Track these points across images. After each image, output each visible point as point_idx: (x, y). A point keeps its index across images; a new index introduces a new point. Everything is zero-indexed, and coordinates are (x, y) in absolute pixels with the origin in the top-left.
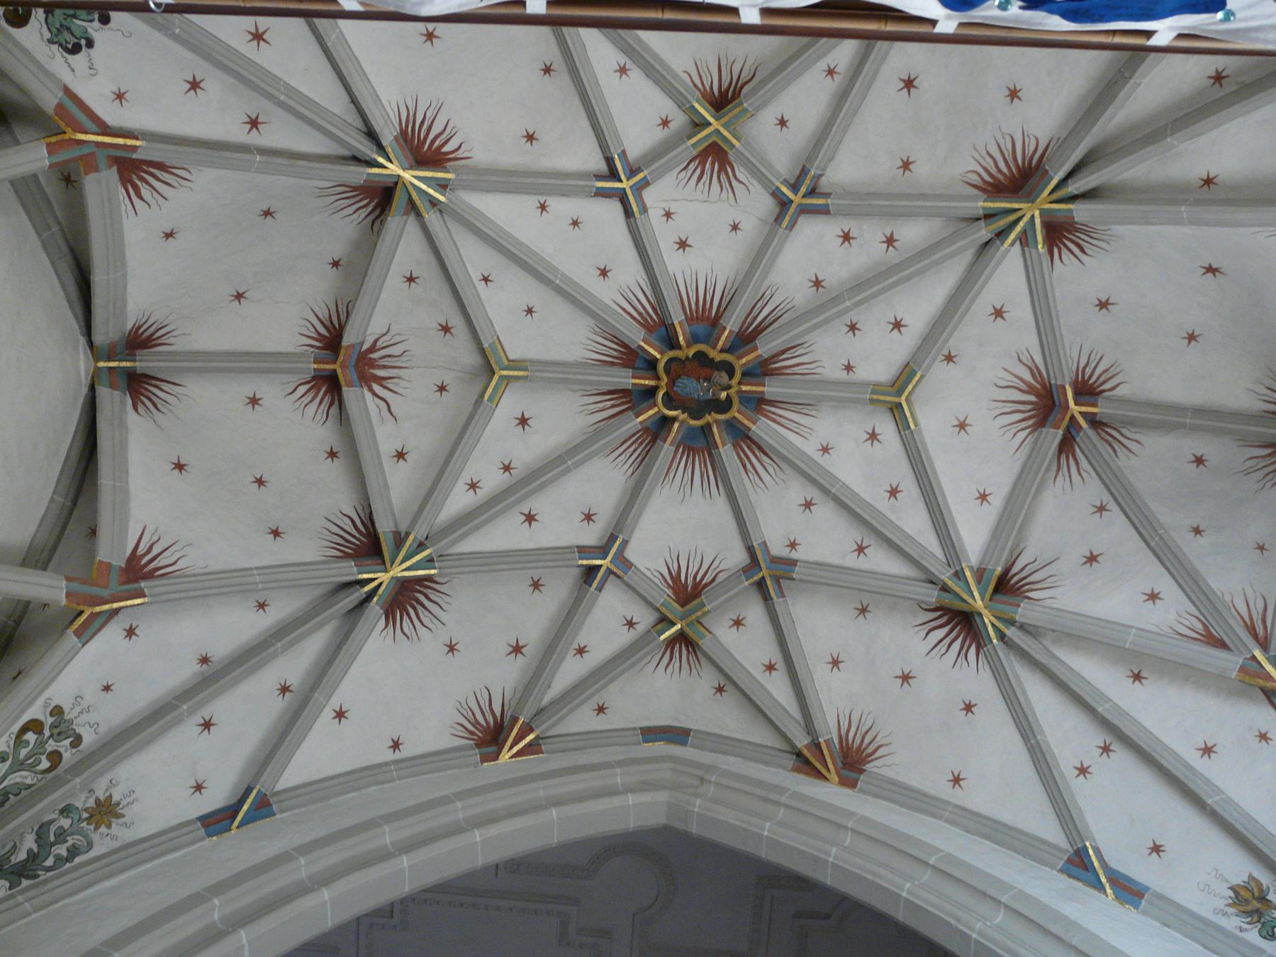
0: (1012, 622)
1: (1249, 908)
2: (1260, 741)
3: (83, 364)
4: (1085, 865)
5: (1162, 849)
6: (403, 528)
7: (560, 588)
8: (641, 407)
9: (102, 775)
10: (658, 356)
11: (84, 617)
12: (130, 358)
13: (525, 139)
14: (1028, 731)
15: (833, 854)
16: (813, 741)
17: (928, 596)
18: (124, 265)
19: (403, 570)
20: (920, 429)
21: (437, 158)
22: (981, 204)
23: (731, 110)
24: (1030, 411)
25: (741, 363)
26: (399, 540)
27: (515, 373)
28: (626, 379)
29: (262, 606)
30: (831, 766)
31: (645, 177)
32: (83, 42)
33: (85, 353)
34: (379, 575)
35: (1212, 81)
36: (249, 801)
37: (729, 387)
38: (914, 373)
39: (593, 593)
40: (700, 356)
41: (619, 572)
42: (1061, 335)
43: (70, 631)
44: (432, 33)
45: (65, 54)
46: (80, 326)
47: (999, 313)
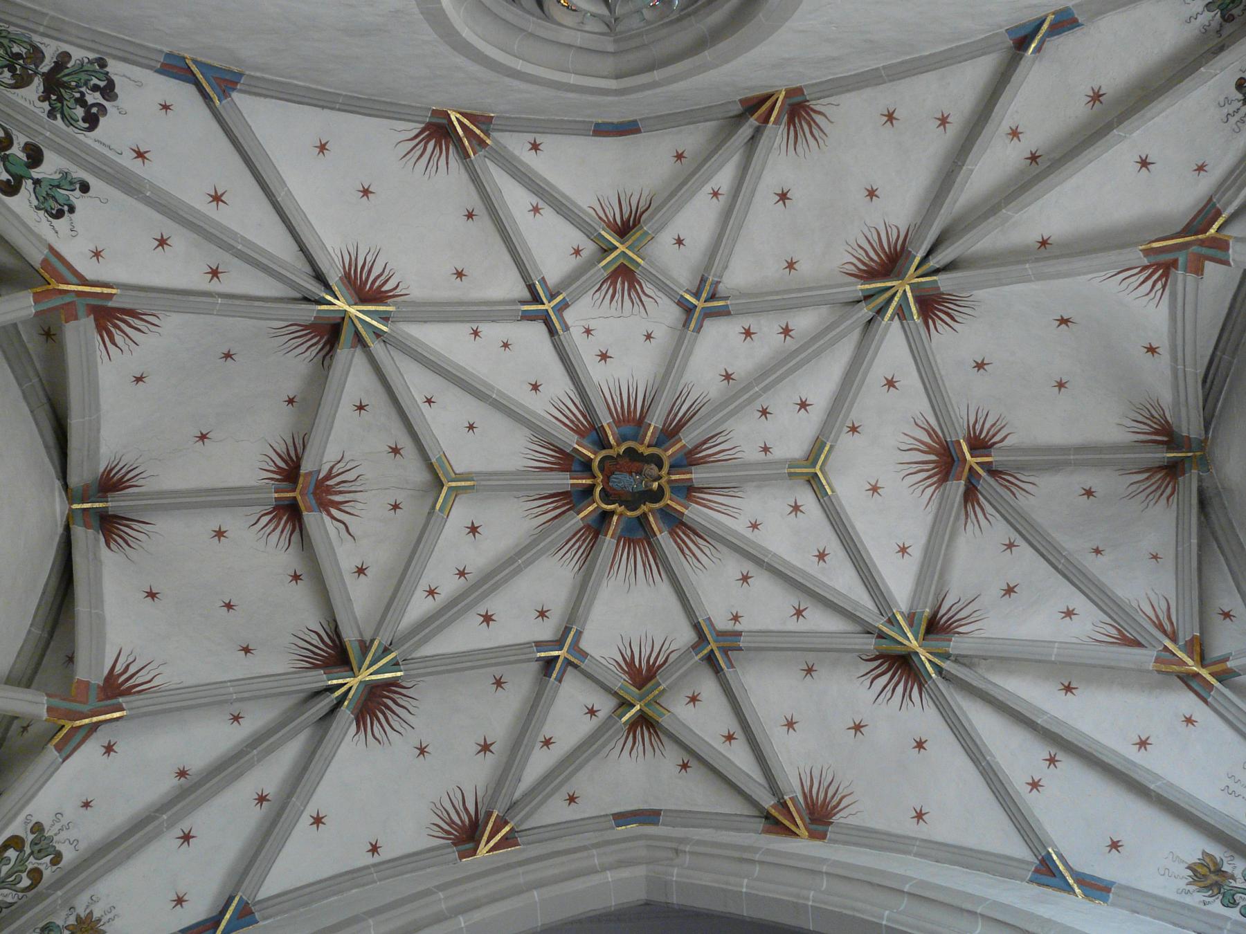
0: (946, 656)
1: (1209, 882)
2: (1187, 725)
3: (58, 506)
4: (1051, 871)
5: (1120, 844)
6: (367, 638)
7: (521, 682)
8: (581, 505)
9: (83, 890)
10: (592, 456)
11: (65, 731)
12: (102, 499)
13: (456, 276)
14: (978, 756)
15: (811, 898)
16: (779, 799)
17: (867, 644)
18: (98, 409)
19: (371, 674)
20: (837, 495)
21: (378, 296)
22: (860, 287)
23: (635, 233)
24: (933, 469)
25: (668, 454)
26: (365, 647)
27: (463, 484)
28: (565, 481)
29: (236, 718)
30: (799, 821)
31: (564, 298)
32: (66, 208)
33: (60, 495)
34: (348, 680)
35: (1030, 161)
36: (232, 908)
37: (660, 478)
38: (824, 444)
39: (554, 683)
40: (630, 452)
41: (576, 661)
42: (948, 396)
43: (51, 746)
44: (368, 189)
45: (50, 219)
46: (56, 472)
47: (891, 383)
